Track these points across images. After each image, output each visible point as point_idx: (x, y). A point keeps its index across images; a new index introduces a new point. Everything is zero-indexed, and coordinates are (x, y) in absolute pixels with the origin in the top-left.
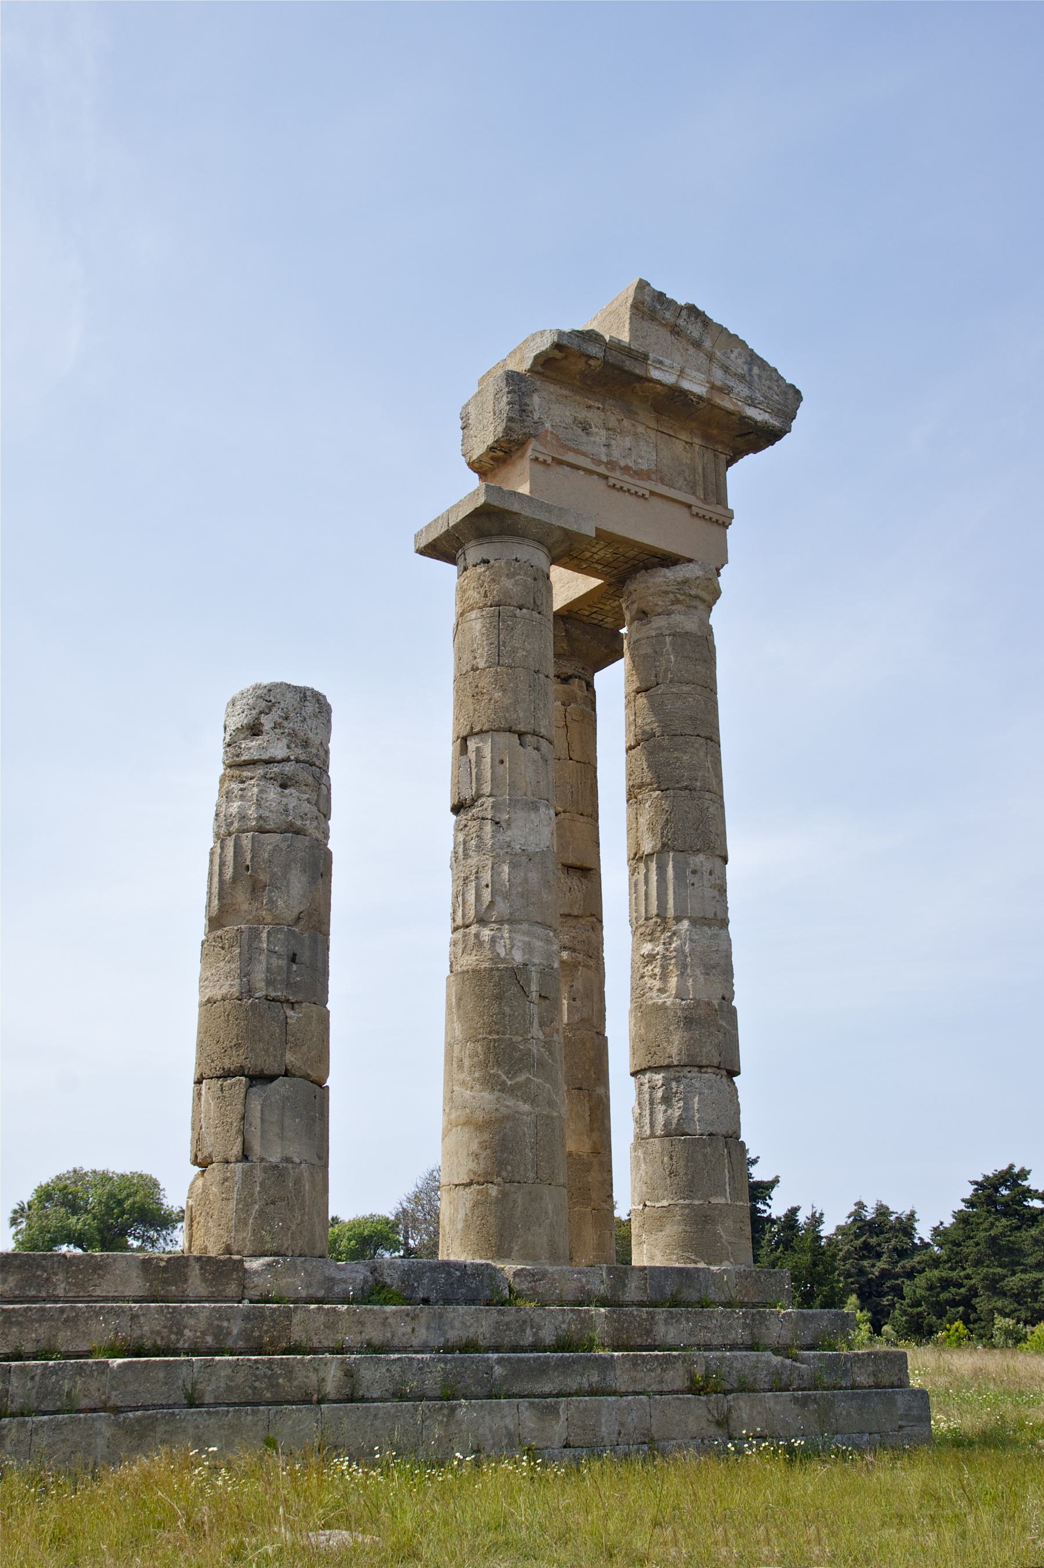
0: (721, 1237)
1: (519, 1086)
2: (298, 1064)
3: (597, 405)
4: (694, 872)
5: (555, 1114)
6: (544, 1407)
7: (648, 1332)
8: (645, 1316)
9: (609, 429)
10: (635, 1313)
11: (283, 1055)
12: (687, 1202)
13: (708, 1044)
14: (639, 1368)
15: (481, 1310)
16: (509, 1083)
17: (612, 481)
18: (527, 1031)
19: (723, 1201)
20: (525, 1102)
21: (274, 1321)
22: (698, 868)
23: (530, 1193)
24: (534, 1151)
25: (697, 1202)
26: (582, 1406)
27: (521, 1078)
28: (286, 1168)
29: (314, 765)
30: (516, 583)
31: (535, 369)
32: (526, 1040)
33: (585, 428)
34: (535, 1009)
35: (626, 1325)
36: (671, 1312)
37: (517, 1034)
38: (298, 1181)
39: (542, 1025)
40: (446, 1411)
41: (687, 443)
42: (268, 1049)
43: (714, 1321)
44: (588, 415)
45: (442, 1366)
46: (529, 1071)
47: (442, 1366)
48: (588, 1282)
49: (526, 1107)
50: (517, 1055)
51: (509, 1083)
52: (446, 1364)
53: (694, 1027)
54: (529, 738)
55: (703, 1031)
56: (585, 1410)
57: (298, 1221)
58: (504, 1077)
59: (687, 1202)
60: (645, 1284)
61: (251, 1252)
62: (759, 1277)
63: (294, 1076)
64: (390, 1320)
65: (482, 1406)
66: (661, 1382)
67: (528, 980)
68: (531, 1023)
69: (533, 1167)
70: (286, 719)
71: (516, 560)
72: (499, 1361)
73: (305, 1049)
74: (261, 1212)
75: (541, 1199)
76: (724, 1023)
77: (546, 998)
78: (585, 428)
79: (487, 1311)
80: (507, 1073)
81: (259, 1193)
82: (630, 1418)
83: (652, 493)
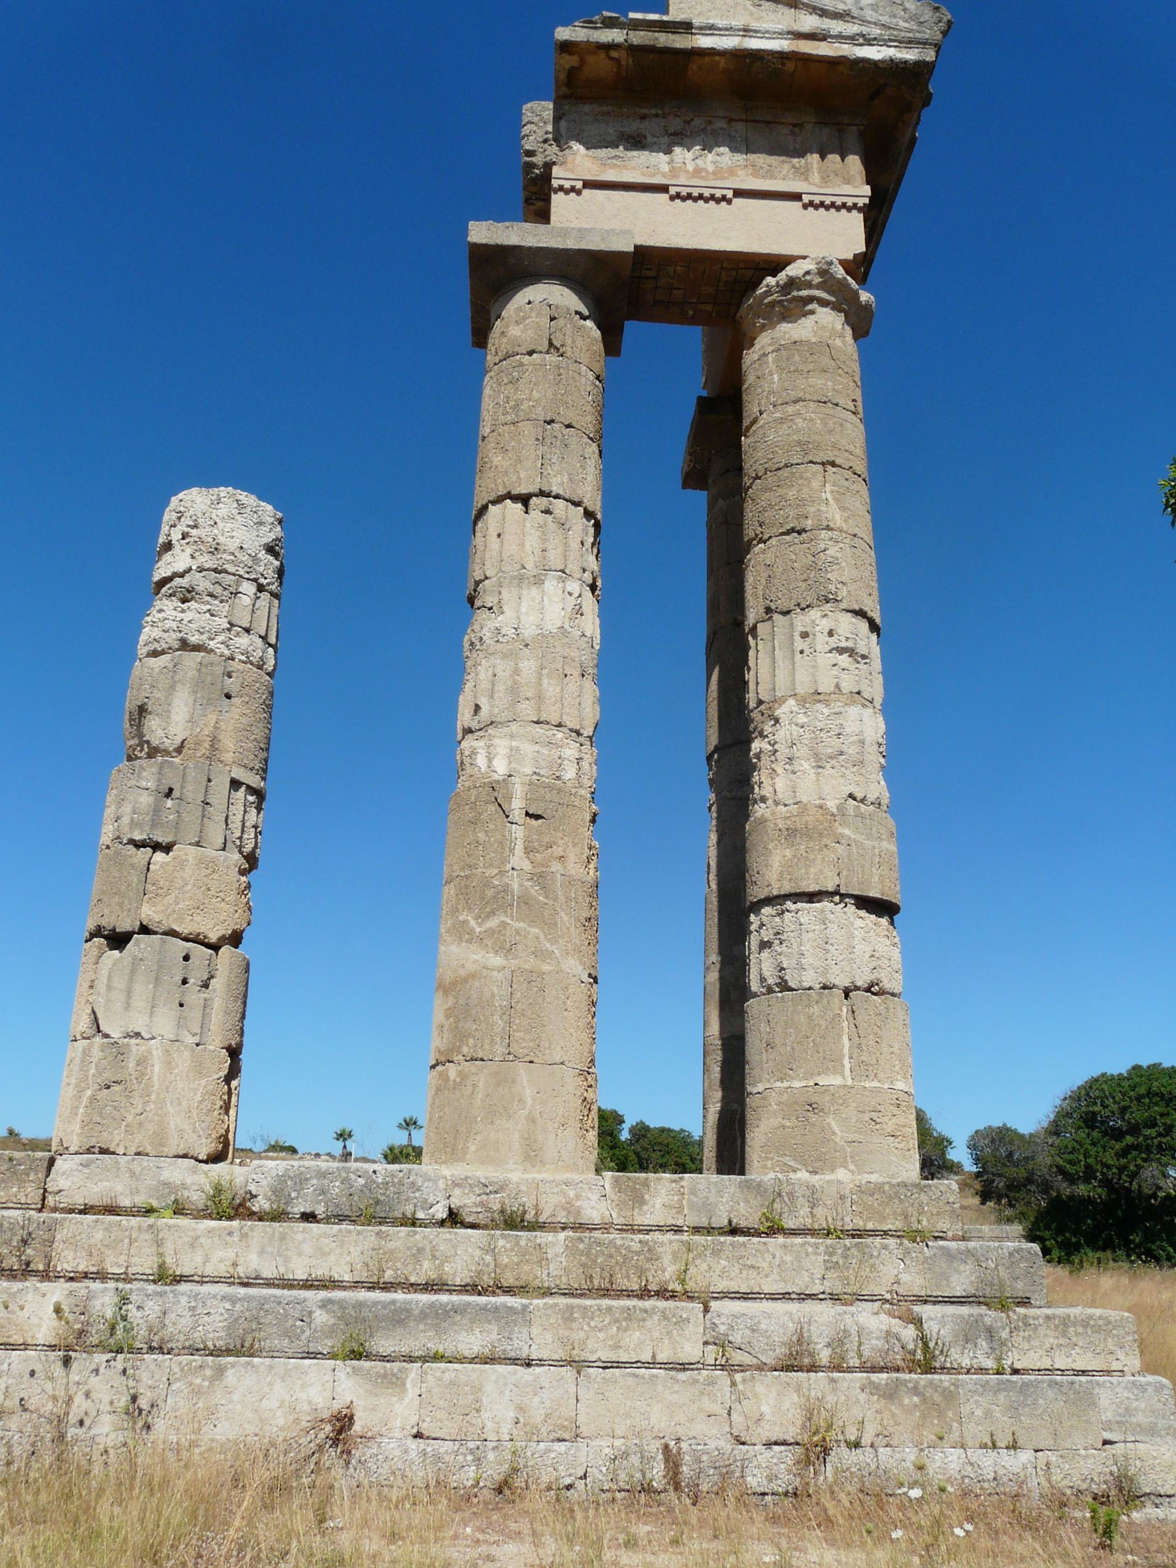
0: (834, 1133)
1: (491, 932)
3: (653, 111)
4: (805, 635)
5: (546, 968)
6: (378, 1375)
8: (636, 1247)
10: (619, 1242)
11: (138, 908)
13: (819, 861)
15: (349, 1232)
16: (478, 930)
17: (673, 190)
18: (506, 861)
19: (836, 1081)
22: (808, 629)
23: (496, 1073)
24: (506, 1017)
26: (447, 1376)
27: (493, 923)
28: (128, 1045)
29: (226, 572)
30: (526, 329)
32: (502, 873)
34: (518, 832)
37: (491, 865)
38: (142, 1061)
39: (528, 851)
40: (208, 1372)
41: (795, 125)
43: (768, 1257)
44: (642, 126)
45: (228, 1306)
47: (228, 1306)
48: (578, 1197)
49: (497, 961)
50: (490, 893)
51: (478, 930)
52: (234, 1303)
54: (534, 501)
55: (811, 844)
56: (452, 1383)
57: (139, 1111)
58: (473, 923)
59: (786, 1084)
60: (680, 1201)
61: (76, 1149)
64: (202, 1240)
65: (271, 1367)
66: (617, 1347)
68: (512, 850)
70: (196, 527)
71: (529, 303)
72: (325, 1304)
73: (170, 899)
74: (93, 1099)
75: (513, 1082)
76: (847, 832)
77: (537, 817)
79: (359, 1233)
80: (477, 917)
82: (537, 1400)
83: (739, 193)
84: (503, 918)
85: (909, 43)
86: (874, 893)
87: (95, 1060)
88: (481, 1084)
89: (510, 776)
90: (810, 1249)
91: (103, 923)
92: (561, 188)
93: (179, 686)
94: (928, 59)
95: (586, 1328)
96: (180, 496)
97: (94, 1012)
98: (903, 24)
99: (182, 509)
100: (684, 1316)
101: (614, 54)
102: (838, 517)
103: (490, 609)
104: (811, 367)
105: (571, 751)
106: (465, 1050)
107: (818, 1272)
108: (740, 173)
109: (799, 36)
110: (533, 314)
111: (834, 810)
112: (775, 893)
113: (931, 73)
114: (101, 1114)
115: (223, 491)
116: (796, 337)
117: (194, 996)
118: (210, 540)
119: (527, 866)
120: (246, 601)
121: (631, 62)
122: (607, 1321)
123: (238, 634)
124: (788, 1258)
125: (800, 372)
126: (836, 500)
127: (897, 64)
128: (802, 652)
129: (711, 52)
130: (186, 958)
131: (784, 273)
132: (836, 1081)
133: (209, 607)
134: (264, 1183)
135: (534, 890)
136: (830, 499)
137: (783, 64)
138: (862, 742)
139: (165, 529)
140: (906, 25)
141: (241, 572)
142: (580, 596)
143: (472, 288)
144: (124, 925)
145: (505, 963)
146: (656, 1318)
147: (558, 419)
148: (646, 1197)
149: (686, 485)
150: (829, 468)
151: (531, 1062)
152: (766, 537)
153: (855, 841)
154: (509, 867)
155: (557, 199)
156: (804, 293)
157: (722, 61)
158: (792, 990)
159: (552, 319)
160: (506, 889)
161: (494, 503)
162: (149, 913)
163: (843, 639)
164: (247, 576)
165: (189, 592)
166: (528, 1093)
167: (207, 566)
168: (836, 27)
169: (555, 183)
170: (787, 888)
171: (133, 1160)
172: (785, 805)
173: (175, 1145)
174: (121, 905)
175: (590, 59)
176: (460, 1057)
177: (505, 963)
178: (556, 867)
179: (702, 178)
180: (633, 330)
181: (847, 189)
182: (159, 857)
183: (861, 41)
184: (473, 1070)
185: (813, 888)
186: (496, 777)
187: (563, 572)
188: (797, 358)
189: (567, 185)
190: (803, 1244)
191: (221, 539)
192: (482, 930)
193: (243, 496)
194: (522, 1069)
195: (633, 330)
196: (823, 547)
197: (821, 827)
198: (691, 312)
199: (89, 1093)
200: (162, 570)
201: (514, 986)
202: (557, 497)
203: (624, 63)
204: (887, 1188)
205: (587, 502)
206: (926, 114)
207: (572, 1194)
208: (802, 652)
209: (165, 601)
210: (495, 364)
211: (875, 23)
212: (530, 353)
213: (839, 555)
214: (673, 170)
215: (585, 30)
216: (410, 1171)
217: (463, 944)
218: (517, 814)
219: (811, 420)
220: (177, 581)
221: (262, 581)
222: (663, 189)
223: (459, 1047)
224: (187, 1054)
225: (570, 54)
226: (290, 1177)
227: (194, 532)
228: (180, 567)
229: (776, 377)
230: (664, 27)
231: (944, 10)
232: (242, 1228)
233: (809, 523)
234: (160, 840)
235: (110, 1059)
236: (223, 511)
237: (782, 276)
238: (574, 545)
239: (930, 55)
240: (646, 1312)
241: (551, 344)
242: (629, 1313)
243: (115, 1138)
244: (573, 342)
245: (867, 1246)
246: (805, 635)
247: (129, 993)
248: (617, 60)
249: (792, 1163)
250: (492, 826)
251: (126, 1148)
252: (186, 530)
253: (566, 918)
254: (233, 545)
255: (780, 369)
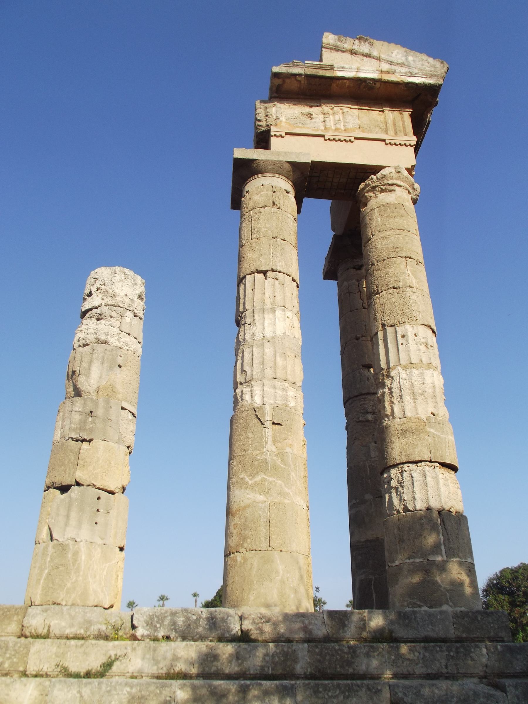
1: (257, 484)
2: (84, 478)
4: (403, 336)
5: (286, 501)
7: (349, 663)
9: (324, 114)
11: (74, 472)
12: (411, 561)
14: (320, 695)
15: (191, 645)
16: (250, 482)
18: (263, 447)
19: (439, 558)
20: (260, 494)
21: (15, 650)
23: (263, 557)
25: (418, 560)
27: (258, 478)
30: (261, 196)
31: (273, 95)
33: (310, 116)
35: (328, 657)
36: (372, 647)
37: (256, 449)
38: (76, 554)
39: (275, 442)
42: (66, 470)
45: (128, 689)
46: (264, 473)
48: (310, 623)
49: (262, 498)
51: (250, 482)
52: (131, 687)
53: (408, 435)
54: (269, 273)
55: (415, 437)
58: (247, 479)
59: (411, 561)
62: (476, 617)
63: (83, 485)
67: (264, 414)
68: (266, 442)
69: (266, 539)
71: (263, 185)
73: (91, 468)
74: (49, 574)
75: (272, 562)
76: (432, 430)
78: (310, 116)
81: (49, 562)
83: (356, 138)
84: (263, 476)
85: (432, 76)
86: (447, 461)
87: (50, 554)
88: (255, 564)
89: (263, 404)
90: (438, 649)
91: (54, 480)
92: (275, 135)
93: (95, 361)
94: (440, 83)
95: (326, 696)
96: (96, 270)
97: (49, 528)
98: (427, 69)
99: (97, 277)
100: (379, 688)
101: (298, 78)
102: (414, 282)
103: (249, 325)
104: (396, 214)
105: (291, 393)
106: (246, 545)
107: (443, 662)
108: (357, 130)
109: (382, 72)
110: (265, 190)
111: (425, 420)
112: (398, 462)
113: (440, 88)
114: (53, 583)
115: (118, 269)
116: (388, 201)
117: (100, 518)
118: (111, 291)
119: (274, 449)
120: (128, 320)
121: (306, 82)
122: (338, 692)
123: (124, 337)
124: (427, 654)
125: (391, 217)
126: (413, 274)
127: (426, 84)
128: (402, 344)
129: (343, 78)
130: (99, 498)
131: (380, 173)
132: (439, 558)
133: (110, 323)
134: (142, 619)
135: (279, 462)
136: (410, 273)
137: (375, 84)
138: (434, 387)
139: (88, 286)
140: (429, 69)
141: (126, 307)
142: (292, 318)
143: (233, 181)
144: (67, 481)
145: (265, 499)
146: (364, 690)
147: (278, 236)
148: (346, 622)
149: (324, 279)
150: (408, 259)
151: (281, 551)
152: (380, 291)
153: (436, 435)
154: (265, 450)
155: (273, 140)
156: (390, 182)
157: (347, 82)
158: (410, 511)
159: (274, 192)
160: (264, 461)
161: (248, 275)
162: (79, 475)
163: (422, 338)
164: (128, 308)
165: (100, 315)
166: (281, 568)
167: (109, 303)
168: (398, 69)
169: (272, 133)
170: (404, 459)
171: (71, 608)
172: (400, 418)
173: (92, 601)
174: (65, 471)
175: (288, 81)
176: (243, 550)
177: (265, 499)
178: (288, 450)
179: (340, 132)
180: (306, 201)
181: (406, 138)
182: (85, 445)
183: (410, 75)
184: (251, 555)
185: (417, 459)
186: (256, 405)
187: (284, 307)
188: (389, 210)
189: (278, 134)
190: (434, 646)
191: (116, 291)
192: (253, 481)
193: (128, 271)
194: (276, 555)
195: (306, 201)
196: (408, 295)
197: (419, 428)
198: (334, 194)
199: (46, 571)
200: (87, 306)
201: (271, 511)
202: (280, 272)
203: (302, 82)
204: (470, 614)
205: (294, 275)
206: (434, 109)
207: (307, 622)
208: (402, 344)
209: (89, 320)
210: (247, 212)
211: (415, 68)
212: (264, 207)
213: (416, 299)
214: (326, 129)
215: (285, 68)
216: (220, 611)
217: (243, 490)
218: (268, 424)
219: (398, 238)
220: (95, 311)
221: (136, 311)
222: (323, 136)
223: (243, 544)
224: (99, 550)
225: (279, 78)
226: (156, 616)
227: (103, 287)
228: (96, 304)
229: (379, 219)
230: (321, 68)
231: (445, 63)
232: (133, 644)
233: (401, 284)
234: (86, 438)
235: (58, 553)
236: (118, 277)
237: (379, 175)
238: (288, 294)
239: (441, 82)
240: (358, 686)
241: (274, 203)
242: (350, 688)
243: (61, 597)
244: (284, 203)
245: (468, 646)
246: (403, 336)
247: (68, 517)
248: (300, 81)
249: (418, 603)
250: (255, 430)
251: (67, 601)
252: (99, 286)
253: (294, 476)
254: (122, 294)
255: (381, 215)
